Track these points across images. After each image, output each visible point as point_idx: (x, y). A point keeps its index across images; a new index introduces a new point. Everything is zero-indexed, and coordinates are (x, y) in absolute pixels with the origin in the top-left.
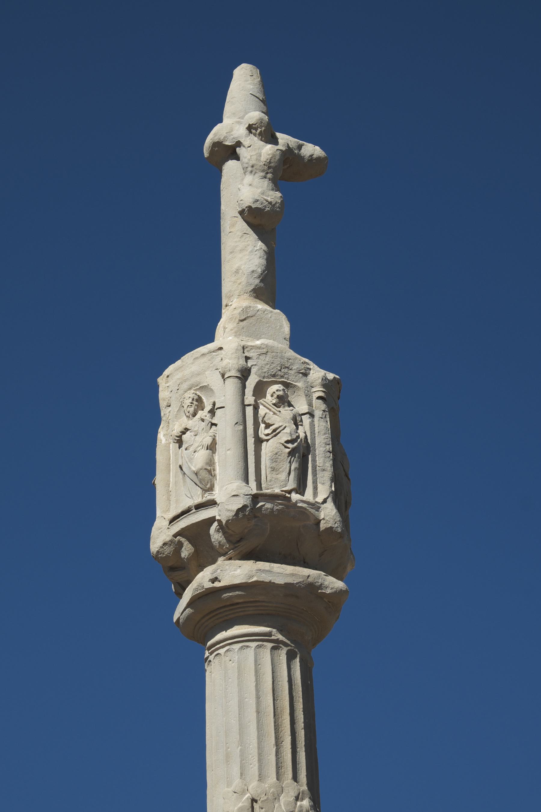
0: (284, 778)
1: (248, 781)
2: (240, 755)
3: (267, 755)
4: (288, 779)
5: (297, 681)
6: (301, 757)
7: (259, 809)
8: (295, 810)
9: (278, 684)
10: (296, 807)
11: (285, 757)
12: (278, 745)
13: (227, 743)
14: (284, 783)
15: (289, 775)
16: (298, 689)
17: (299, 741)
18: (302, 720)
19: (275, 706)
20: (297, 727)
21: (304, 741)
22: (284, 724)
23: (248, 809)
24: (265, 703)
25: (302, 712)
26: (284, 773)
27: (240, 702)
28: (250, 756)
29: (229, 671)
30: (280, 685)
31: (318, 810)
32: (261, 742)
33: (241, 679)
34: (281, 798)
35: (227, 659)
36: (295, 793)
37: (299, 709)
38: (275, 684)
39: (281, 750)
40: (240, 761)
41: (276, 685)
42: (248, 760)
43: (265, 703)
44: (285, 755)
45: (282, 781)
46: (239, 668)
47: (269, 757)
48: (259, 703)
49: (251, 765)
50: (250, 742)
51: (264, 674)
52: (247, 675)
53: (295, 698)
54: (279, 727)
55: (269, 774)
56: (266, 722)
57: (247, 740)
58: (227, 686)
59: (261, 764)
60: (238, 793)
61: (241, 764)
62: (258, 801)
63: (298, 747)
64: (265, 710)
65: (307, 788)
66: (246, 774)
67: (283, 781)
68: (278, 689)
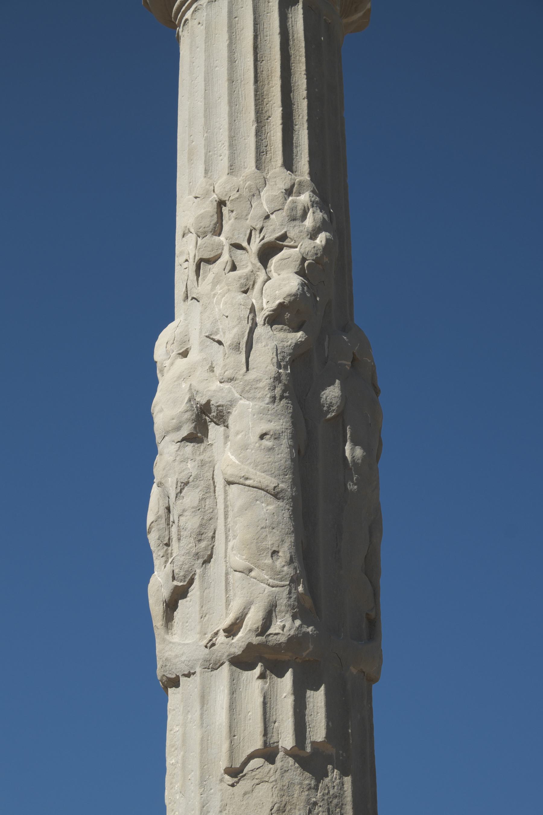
0: (269, 167)
1: (216, 179)
2: (204, 145)
3: (243, 138)
4: (276, 167)
5: (297, 34)
6: (300, 137)
7: (229, 213)
8: (284, 207)
9: (265, 39)
10: (286, 203)
11: (272, 138)
12: (261, 122)
13: (191, 136)
14: (269, 174)
15: (278, 161)
16: (299, 45)
17: (299, 116)
18: (305, 86)
19: (258, 68)
20: (295, 97)
21: (307, 114)
22: (272, 92)
23: (212, 216)
24: (243, 67)
25: (305, 76)
26: (270, 160)
27: (208, 74)
28: (219, 144)
29: (197, 38)
30: (268, 40)
31: (332, 211)
32: (235, 121)
33: (209, 42)
34: (262, 194)
35: (196, 22)
36: (286, 185)
37: (299, 72)
38: (259, 40)
39: (266, 129)
40: (205, 153)
41: (261, 40)
42: (216, 150)
43: (243, 67)
44: (272, 135)
45: (267, 170)
46: (208, 28)
47: (246, 141)
48: (233, 69)
49: (220, 156)
50: (220, 125)
51: (243, 29)
52: (219, 36)
53: (294, 57)
54: (264, 97)
55: (246, 163)
56: (243, 93)
57: (216, 124)
58: (194, 58)
59: (234, 151)
60: (199, 197)
61: (206, 157)
62: (227, 202)
63: (297, 123)
64: (242, 77)
65: (309, 179)
66: (213, 170)
67: (268, 171)
68: (264, 45)
